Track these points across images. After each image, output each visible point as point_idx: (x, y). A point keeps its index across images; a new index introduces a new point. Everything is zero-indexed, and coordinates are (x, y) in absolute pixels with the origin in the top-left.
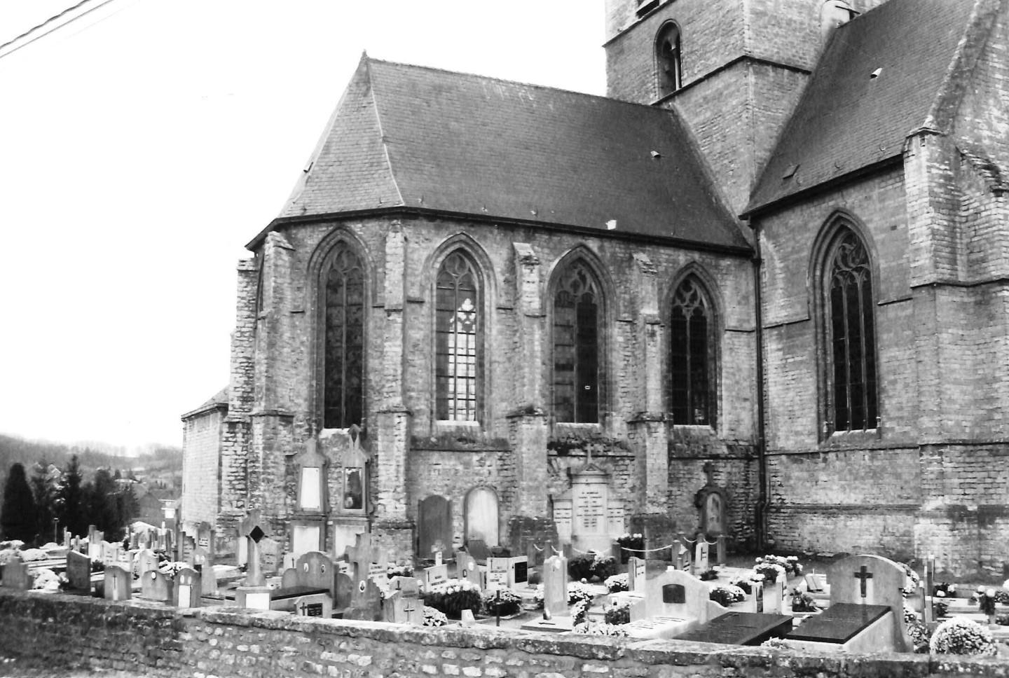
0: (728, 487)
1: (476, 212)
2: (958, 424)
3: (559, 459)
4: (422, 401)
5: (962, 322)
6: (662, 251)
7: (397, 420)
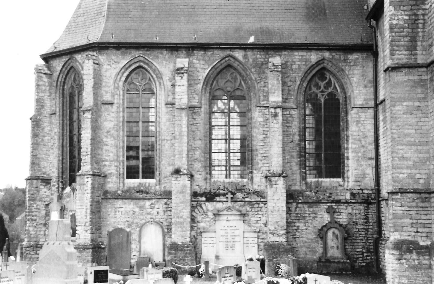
0: (349, 224)
1: (150, 41)
2: (410, 176)
3: (207, 203)
4: (113, 167)
5: (419, 96)
6: (296, 53)
7: (86, 180)
